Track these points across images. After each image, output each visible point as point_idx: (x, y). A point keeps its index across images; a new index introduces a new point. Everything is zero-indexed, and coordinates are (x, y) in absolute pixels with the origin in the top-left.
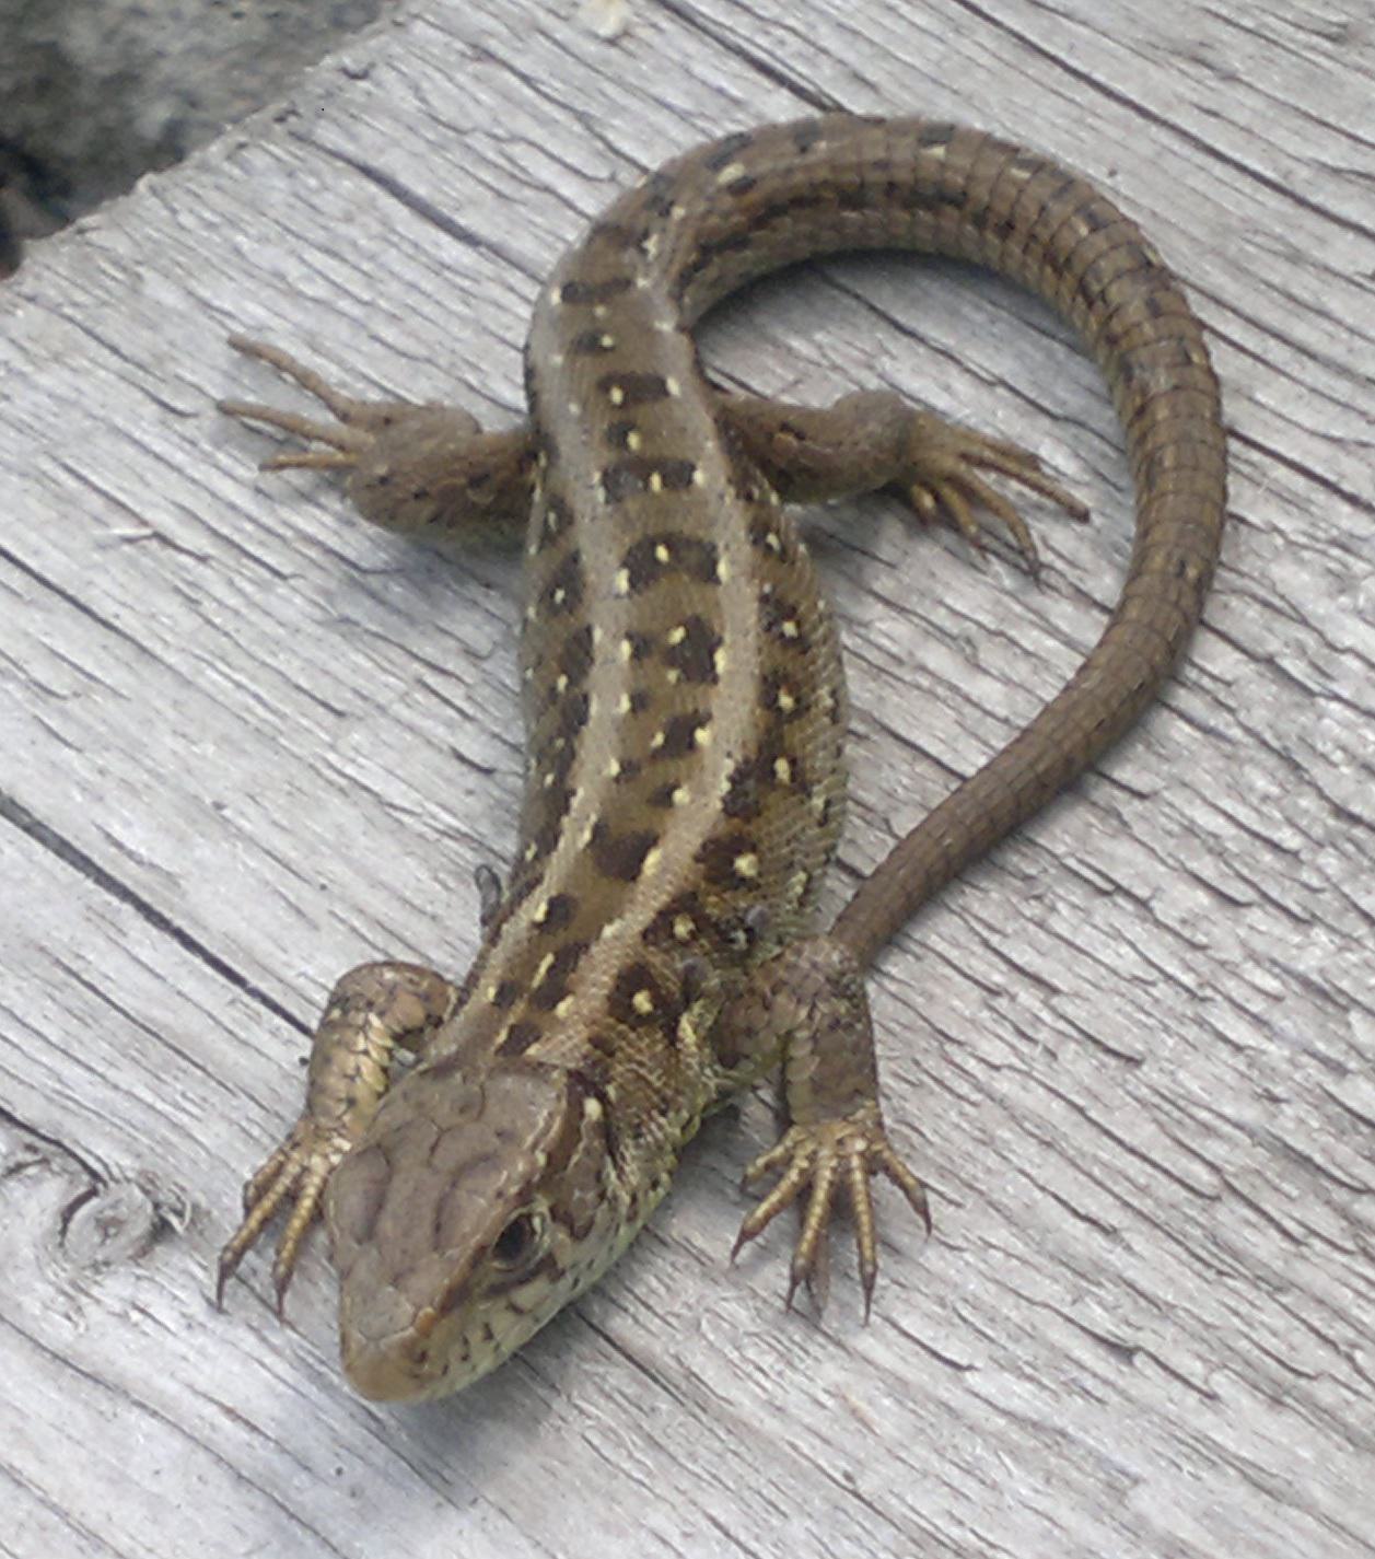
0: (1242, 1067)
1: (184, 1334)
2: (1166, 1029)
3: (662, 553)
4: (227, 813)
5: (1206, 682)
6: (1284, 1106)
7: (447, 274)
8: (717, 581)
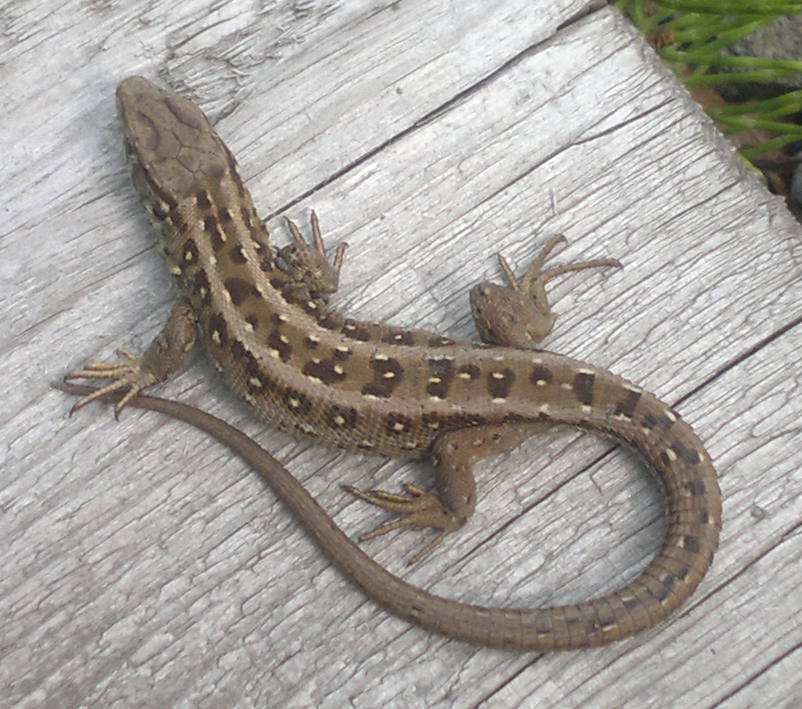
0: (150, 586)
1: (92, 165)
2: (178, 561)
3: (390, 375)
4: (378, 221)
5: (376, 620)
6: (125, 597)
7: (703, 358)
8: (364, 393)
